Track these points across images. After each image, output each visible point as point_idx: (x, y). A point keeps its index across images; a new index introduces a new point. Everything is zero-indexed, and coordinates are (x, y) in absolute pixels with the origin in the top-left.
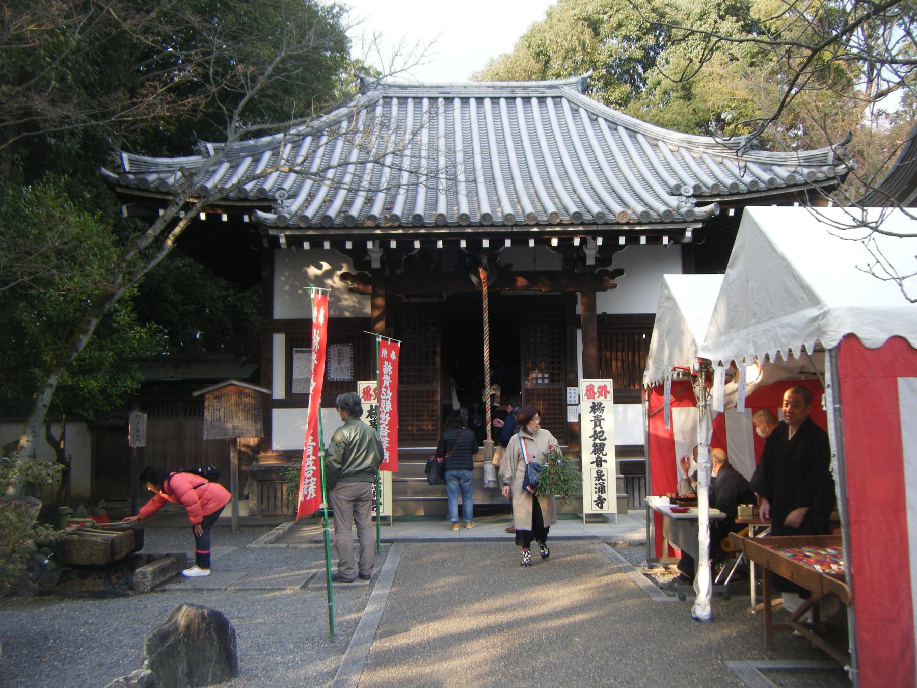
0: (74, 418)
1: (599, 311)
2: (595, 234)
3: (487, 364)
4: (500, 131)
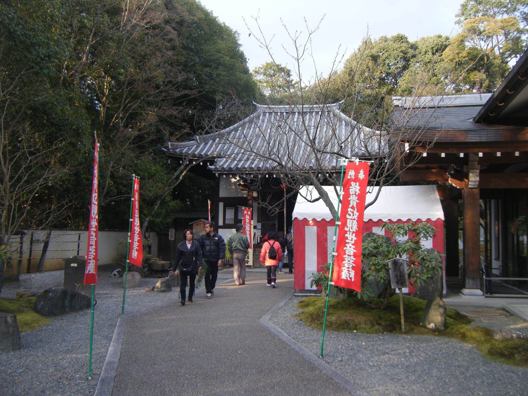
0: (153, 230)
3: (285, 215)
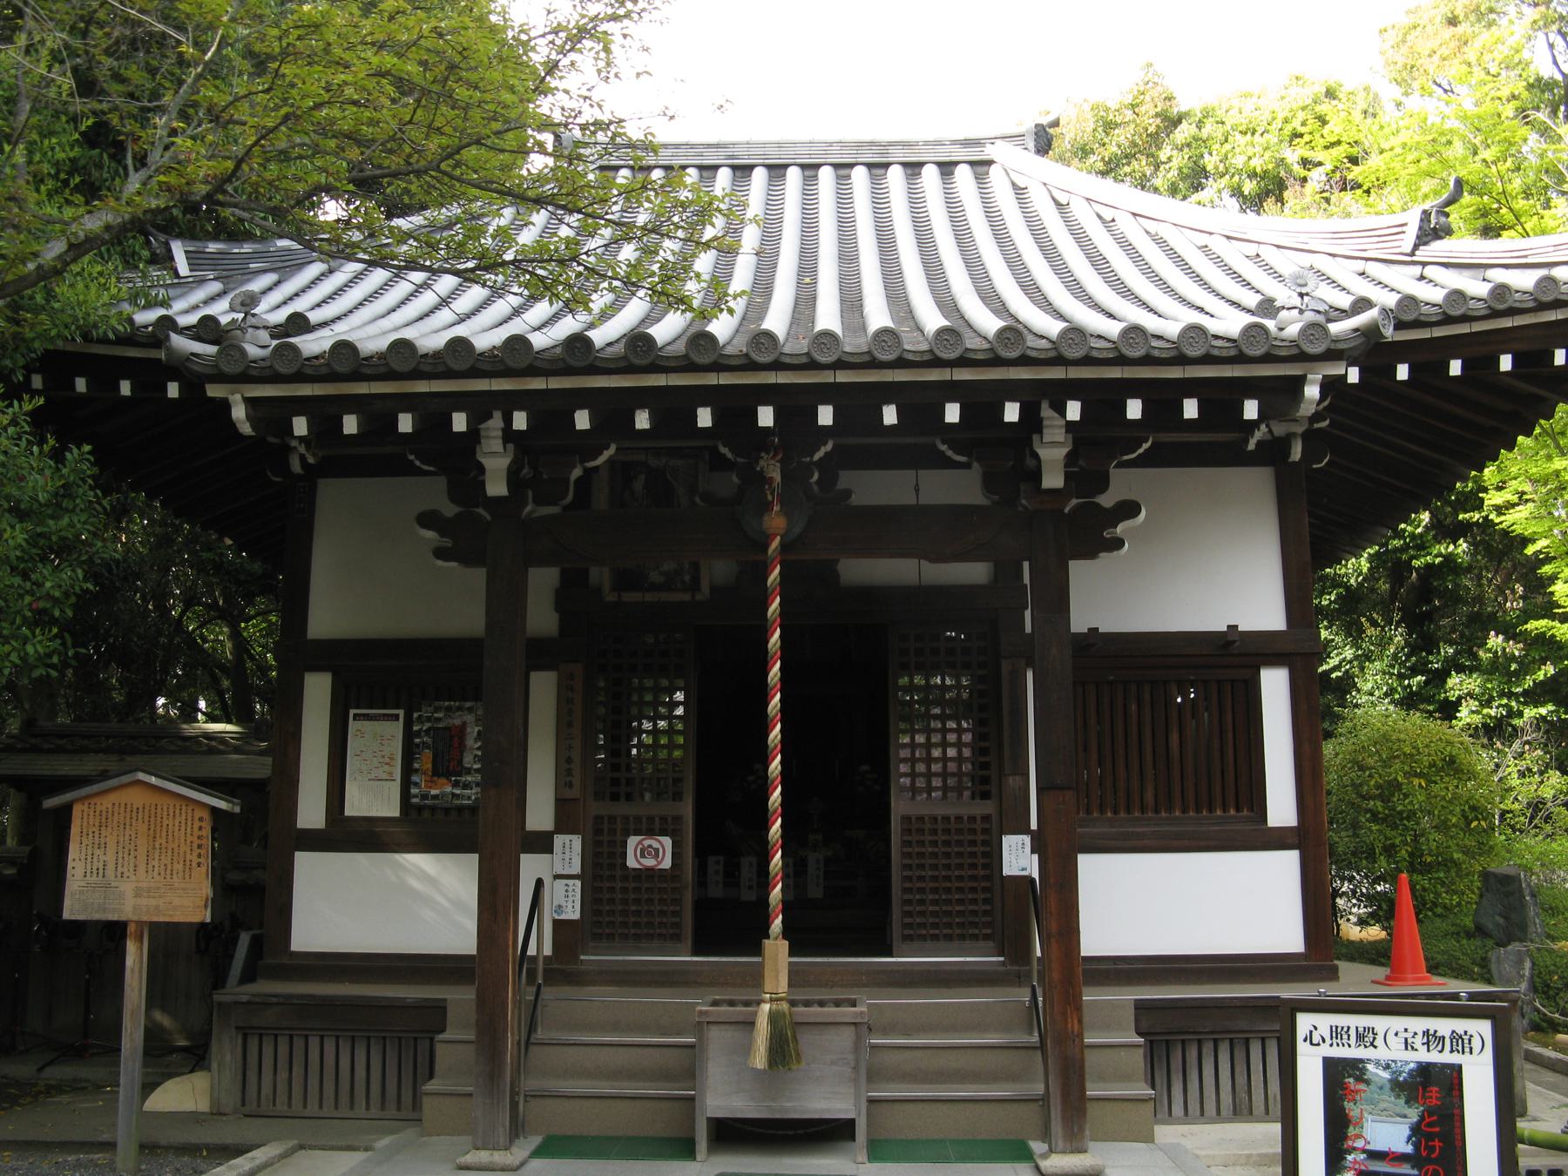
1: (1081, 620)
2: (1059, 393)
4: (846, 226)
